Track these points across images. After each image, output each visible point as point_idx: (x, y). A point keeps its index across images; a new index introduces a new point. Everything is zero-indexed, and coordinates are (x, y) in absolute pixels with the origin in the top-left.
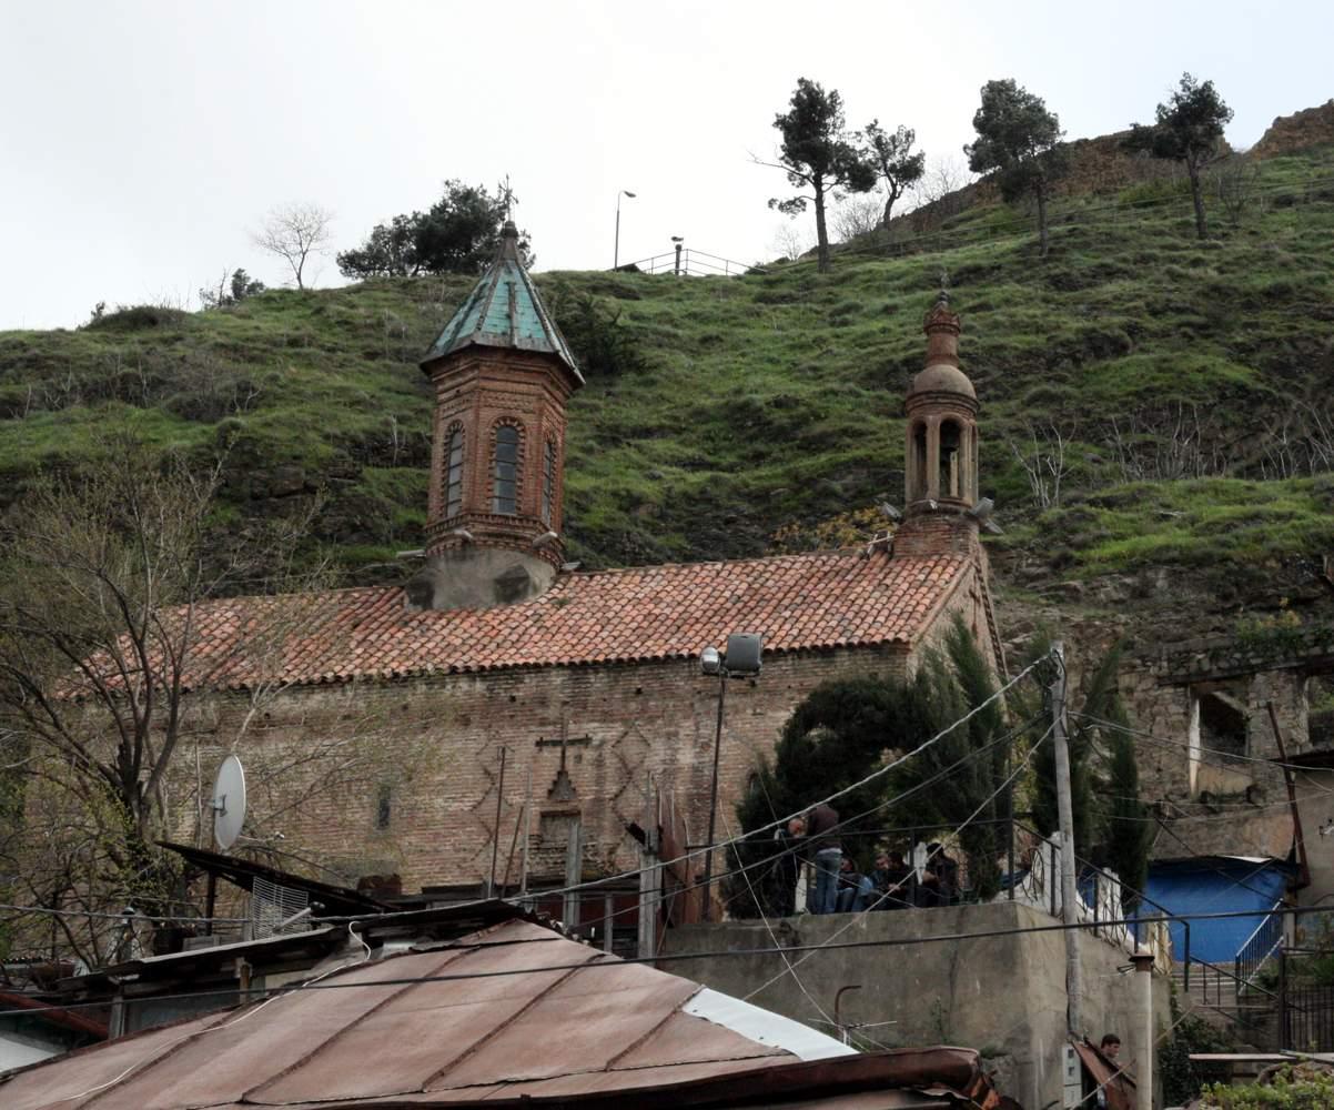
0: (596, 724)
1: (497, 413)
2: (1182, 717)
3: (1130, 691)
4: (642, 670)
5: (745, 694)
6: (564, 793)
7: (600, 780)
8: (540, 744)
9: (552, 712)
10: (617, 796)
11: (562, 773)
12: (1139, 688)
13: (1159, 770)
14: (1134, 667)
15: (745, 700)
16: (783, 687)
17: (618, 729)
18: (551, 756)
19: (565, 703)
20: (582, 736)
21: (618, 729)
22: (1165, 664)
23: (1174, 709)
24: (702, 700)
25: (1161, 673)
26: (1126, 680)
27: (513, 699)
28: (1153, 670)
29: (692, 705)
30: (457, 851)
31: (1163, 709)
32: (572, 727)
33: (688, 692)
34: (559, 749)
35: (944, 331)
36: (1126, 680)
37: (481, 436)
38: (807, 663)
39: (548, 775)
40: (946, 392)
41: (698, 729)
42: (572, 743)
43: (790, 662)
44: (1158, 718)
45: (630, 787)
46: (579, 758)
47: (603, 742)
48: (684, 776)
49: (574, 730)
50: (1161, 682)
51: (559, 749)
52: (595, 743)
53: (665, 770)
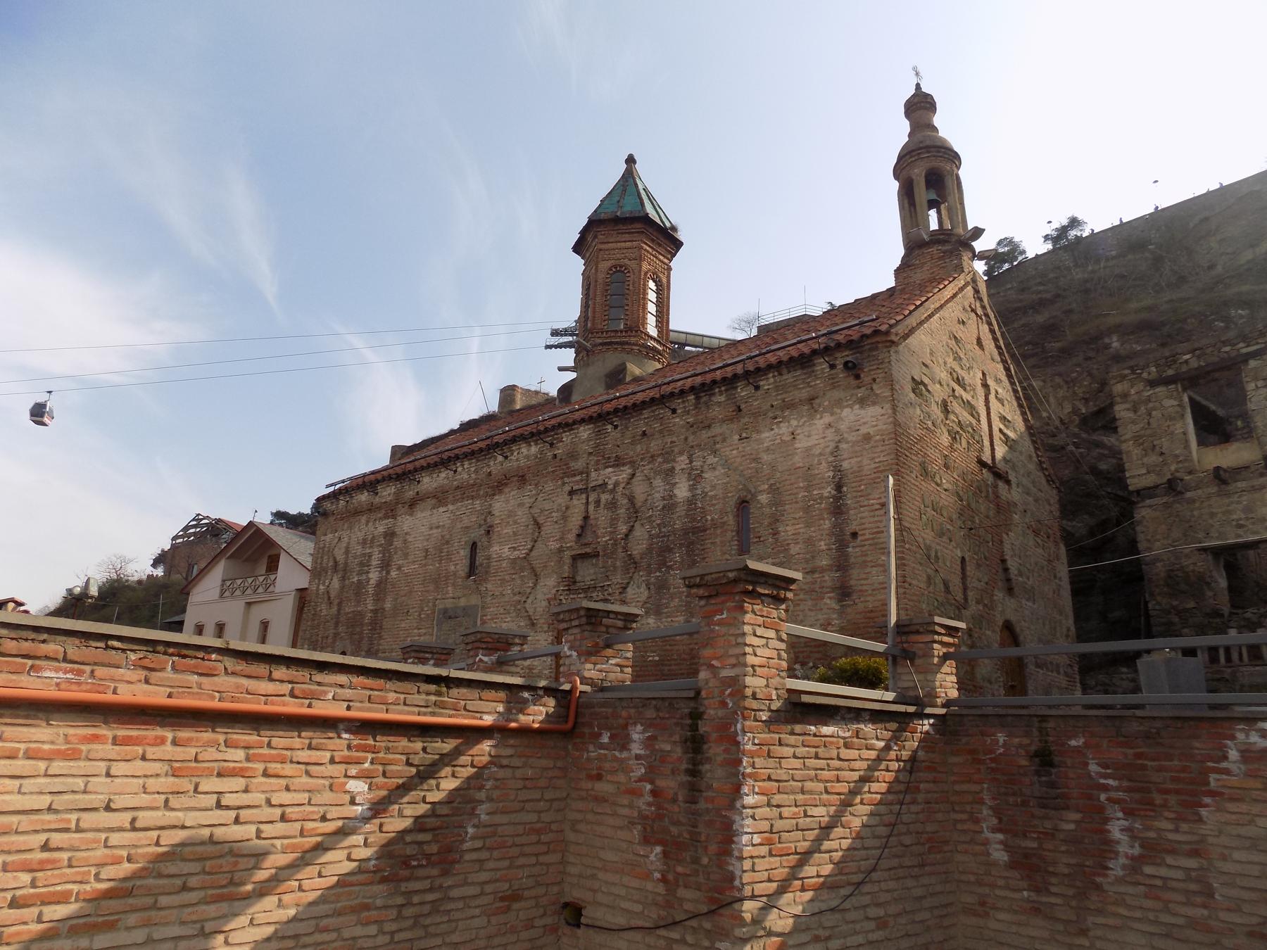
0: (610, 470)
1: (609, 264)
2: (1178, 409)
3: (1125, 396)
4: (646, 413)
5: (731, 420)
6: (589, 538)
7: (613, 522)
8: (572, 493)
9: (579, 465)
10: (627, 535)
11: (586, 518)
12: (1133, 392)
13: (1162, 454)
14: (1126, 376)
15: (732, 426)
16: (766, 406)
17: (627, 470)
18: (578, 502)
19: (590, 454)
20: (600, 482)
21: (627, 470)
22: (1153, 369)
23: (1169, 403)
24: (694, 433)
25: (1150, 377)
26: (1118, 388)
27: (555, 456)
28: (1145, 375)
29: (686, 439)
30: (515, 595)
31: (1157, 404)
32: (593, 475)
33: (683, 427)
34: (584, 496)
35: (921, 108)
36: (1118, 388)
37: (600, 281)
38: (788, 377)
39: (575, 521)
40: (927, 147)
41: (691, 462)
42: (594, 489)
43: (772, 380)
44: (1154, 413)
45: (637, 525)
46: (598, 502)
47: (616, 484)
48: (681, 510)
49: (596, 478)
50: (1152, 384)
51: (584, 496)
52: (610, 487)
53: (664, 507)
